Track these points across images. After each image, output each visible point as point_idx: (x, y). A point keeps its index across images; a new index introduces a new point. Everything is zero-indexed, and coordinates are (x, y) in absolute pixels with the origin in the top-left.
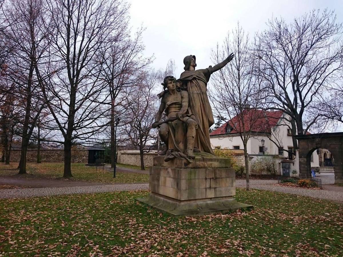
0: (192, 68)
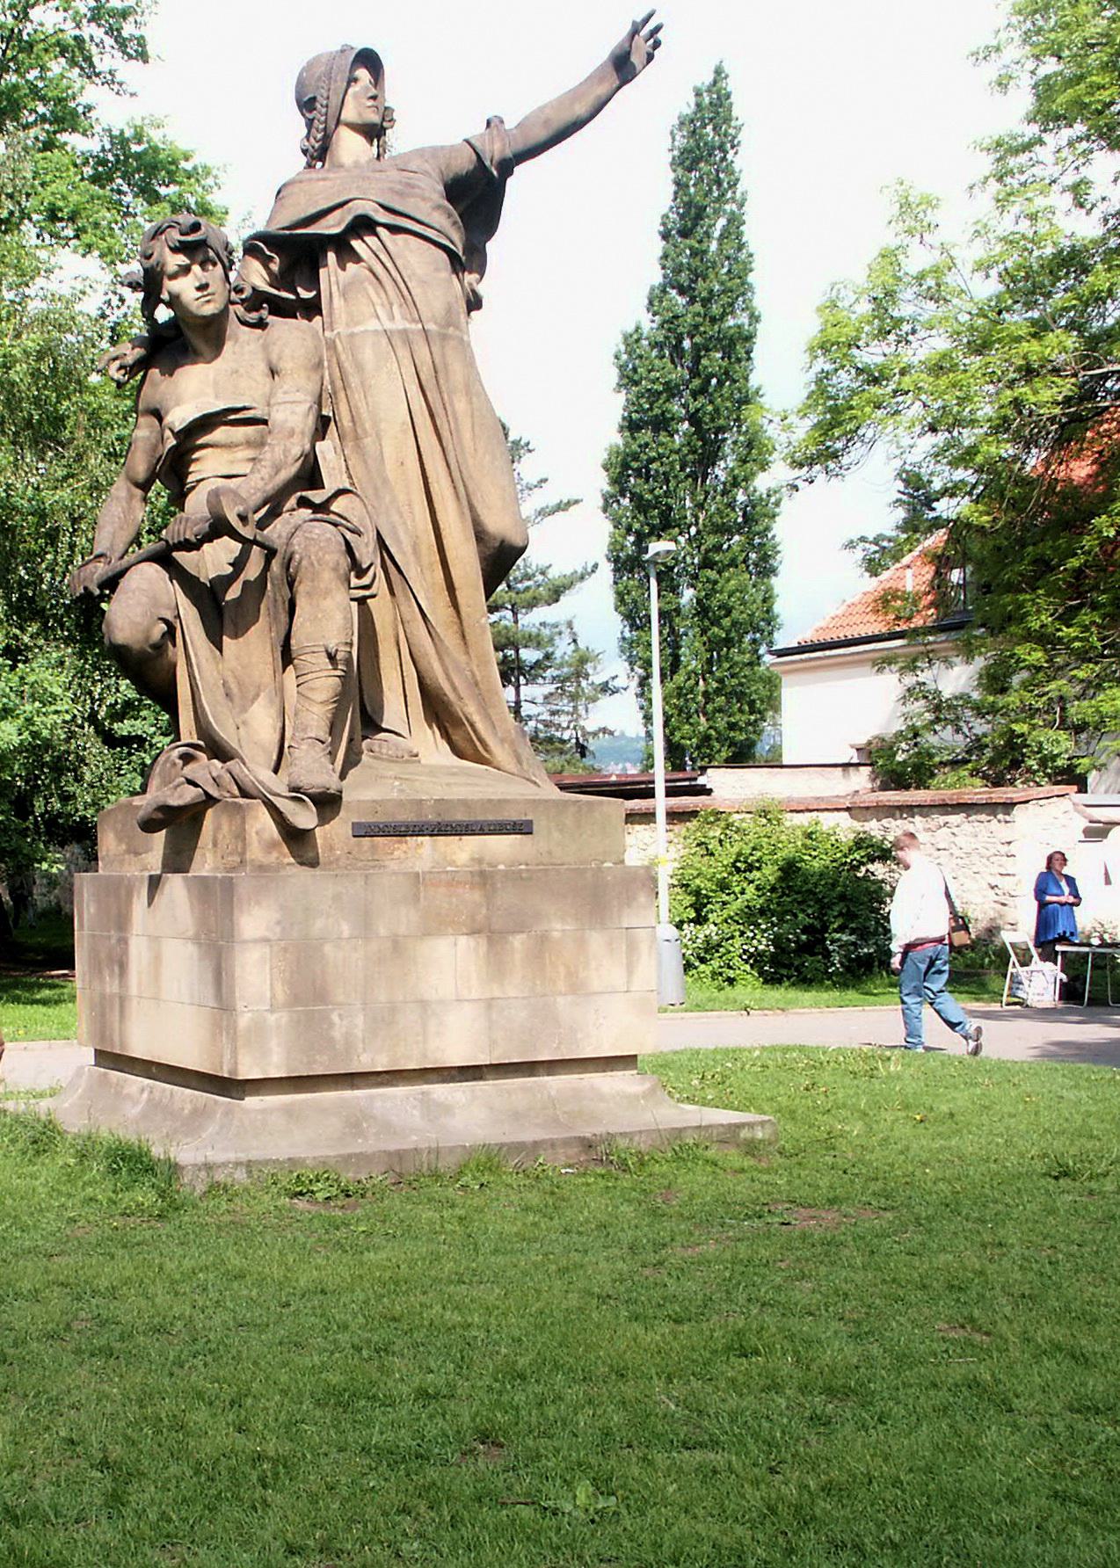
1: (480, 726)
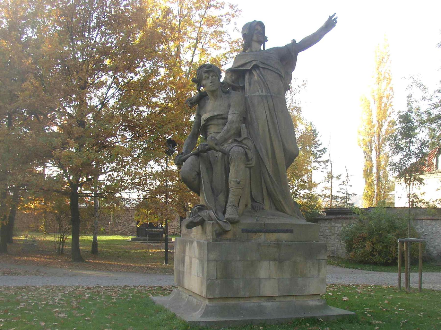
0: (255, 45)
1: (282, 202)
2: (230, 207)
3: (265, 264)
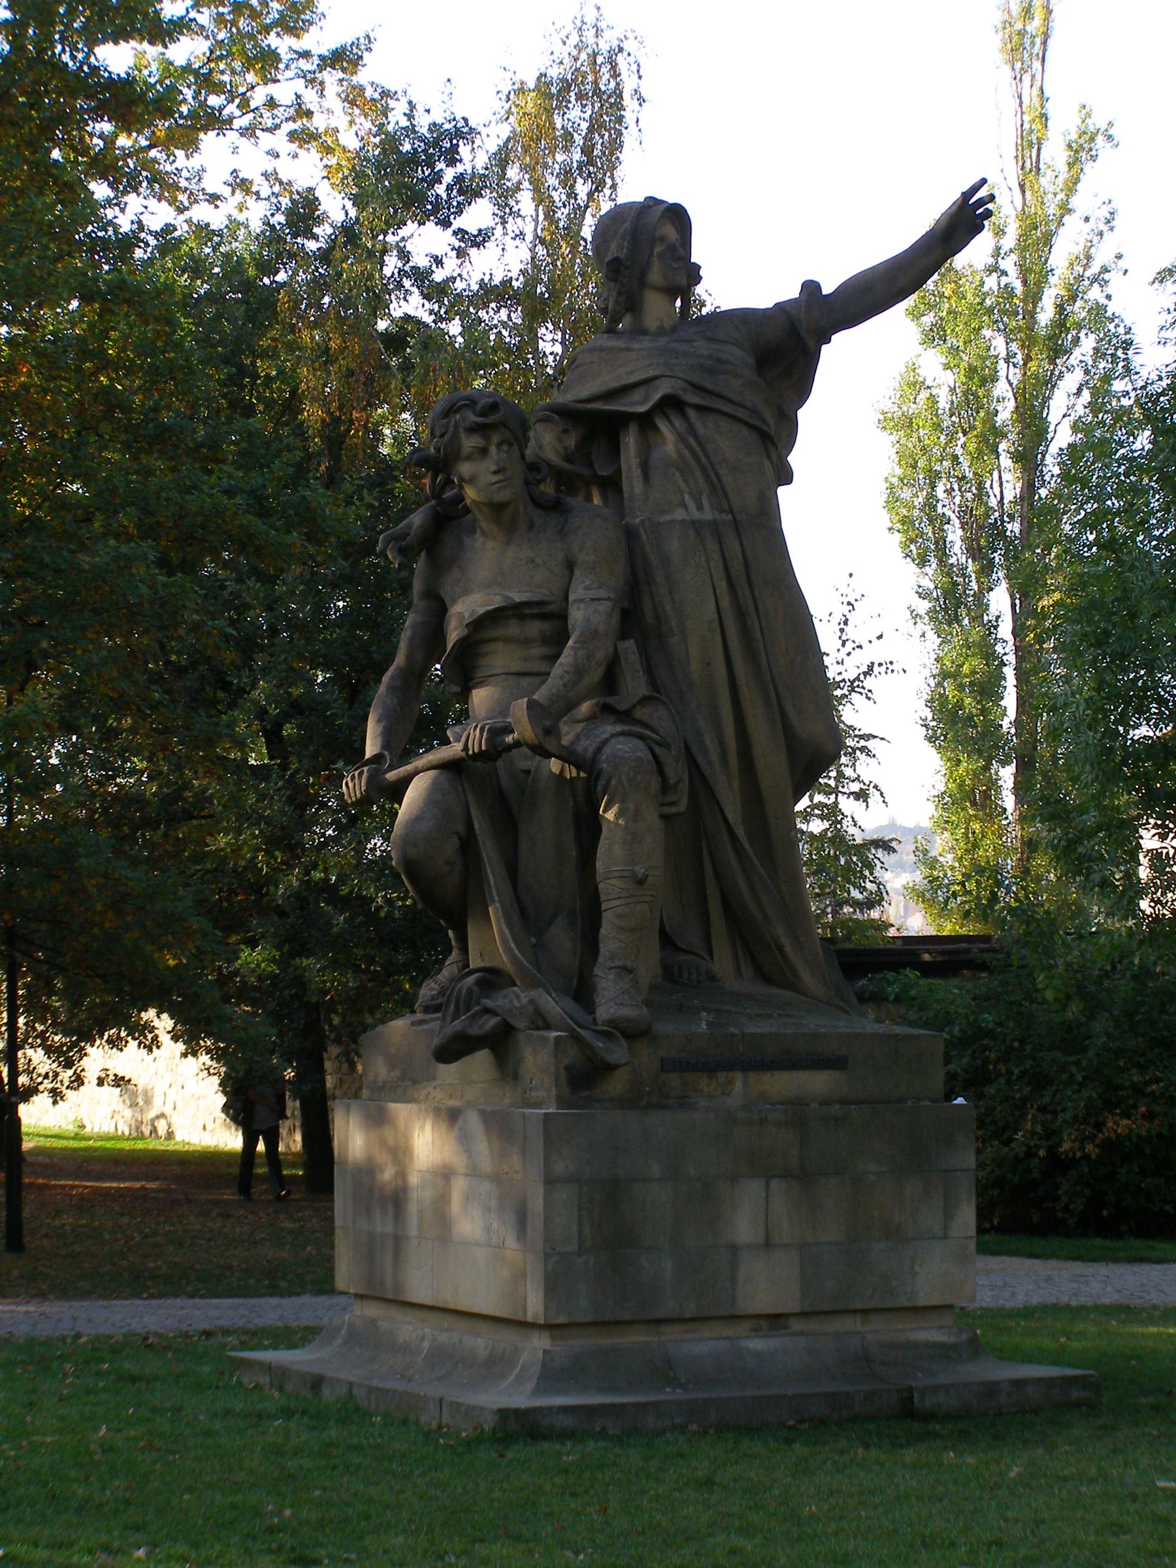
1: (788, 949)
2: (611, 977)
3: (751, 1192)
